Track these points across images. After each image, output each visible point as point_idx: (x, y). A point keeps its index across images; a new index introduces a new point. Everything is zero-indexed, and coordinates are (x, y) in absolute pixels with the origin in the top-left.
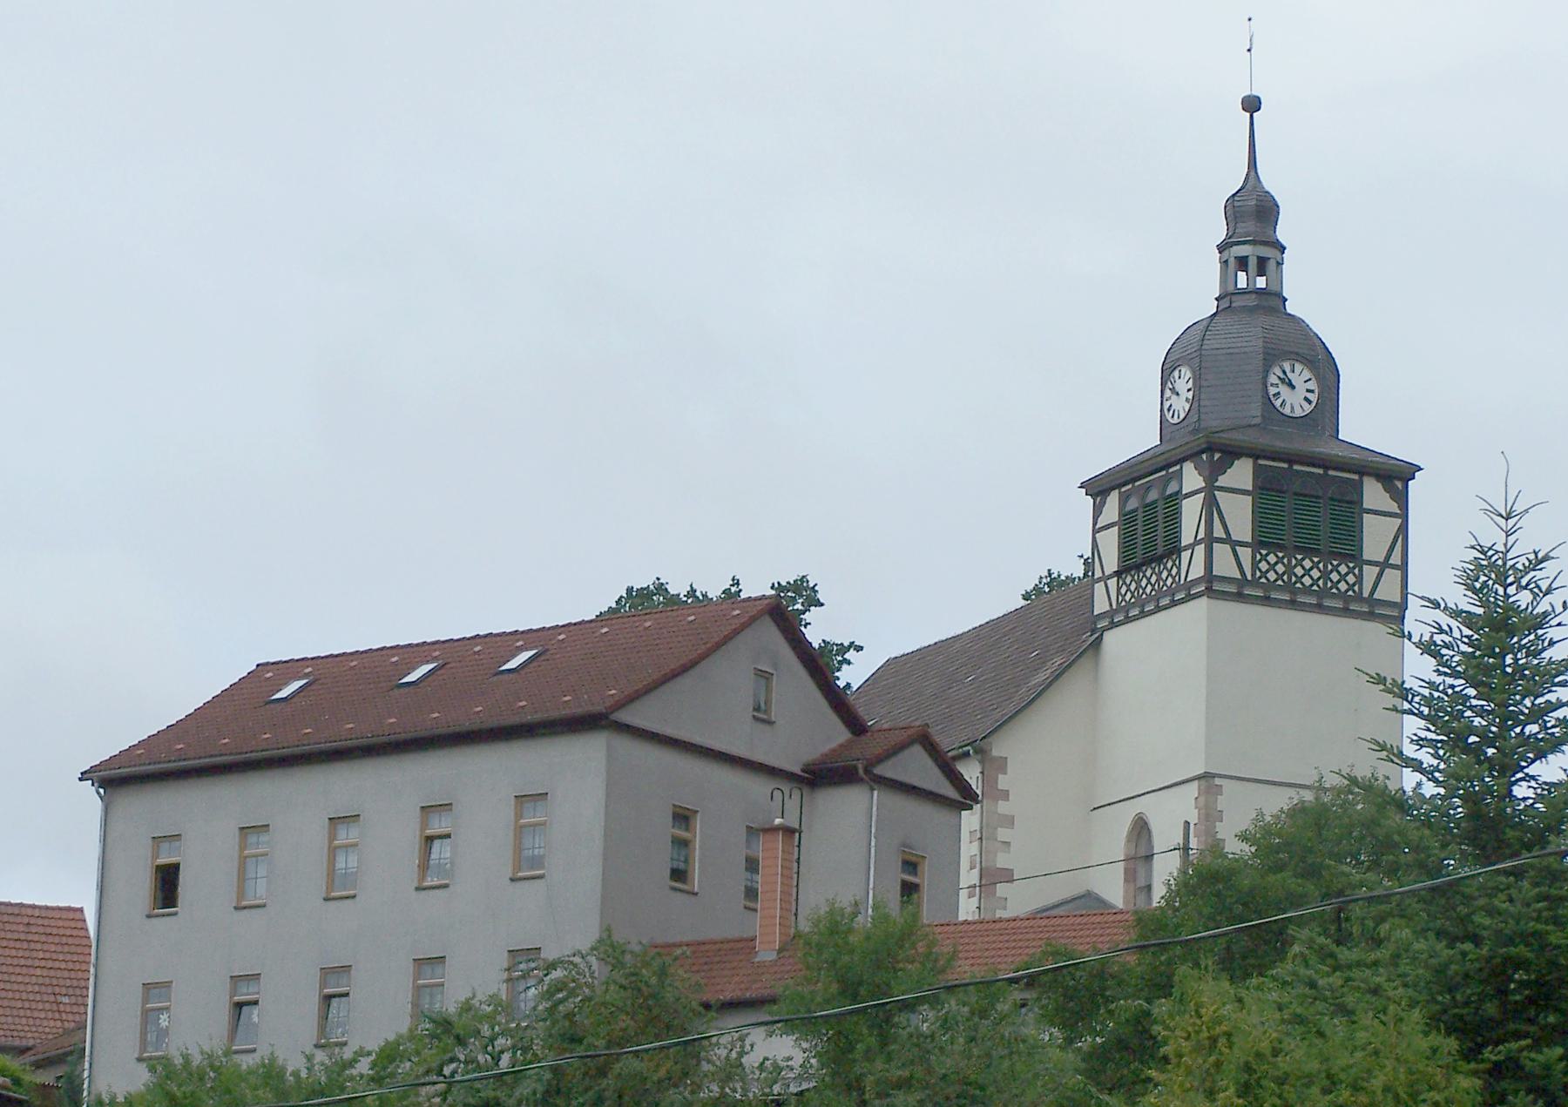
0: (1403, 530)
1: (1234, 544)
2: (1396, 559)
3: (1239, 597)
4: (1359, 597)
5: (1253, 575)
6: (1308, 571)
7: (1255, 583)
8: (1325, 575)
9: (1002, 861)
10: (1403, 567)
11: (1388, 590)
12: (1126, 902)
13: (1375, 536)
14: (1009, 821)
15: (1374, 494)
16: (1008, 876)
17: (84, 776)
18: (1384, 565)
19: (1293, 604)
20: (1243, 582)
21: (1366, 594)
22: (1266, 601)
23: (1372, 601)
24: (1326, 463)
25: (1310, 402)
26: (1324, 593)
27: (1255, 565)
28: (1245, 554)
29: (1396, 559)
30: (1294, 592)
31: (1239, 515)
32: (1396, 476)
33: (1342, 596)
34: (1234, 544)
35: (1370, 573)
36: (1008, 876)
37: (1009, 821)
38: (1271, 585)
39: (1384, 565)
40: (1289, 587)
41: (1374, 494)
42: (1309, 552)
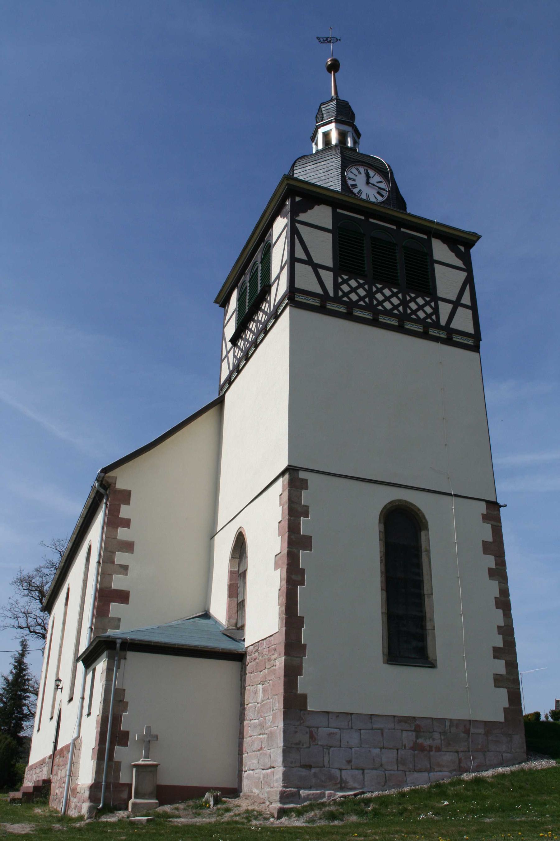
0: (469, 281)
1: (316, 267)
2: (466, 299)
3: (322, 309)
4: (436, 325)
5: (336, 292)
6: (388, 298)
7: (337, 299)
8: (404, 303)
9: (118, 582)
10: (474, 307)
11: (463, 321)
12: (229, 618)
13: (447, 282)
14: (128, 547)
15: (440, 251)
16: (123, 597)
17: (432, 665)
18: (457, 304)
19: (375, 323)
20: (324, 297)
21: (443, 322)
22: (349, 316)
23: (447, 328)
24: (400, 223)
25: (382, 196)
26: (403, 318)
27: (337, 286)
28: (328, 277)
29: (466, 299)
30: (376, 313)
31: (323, 248)
32: (462, 243)
33: (418, 321)
34: (316, 267)
35: (445, 309)
36: (123, 597)
37: (128, 547)
38: (354, 305)
39: (457, 304)
40: (369, 307)
41: (440, 251)
42: (389, 282)
